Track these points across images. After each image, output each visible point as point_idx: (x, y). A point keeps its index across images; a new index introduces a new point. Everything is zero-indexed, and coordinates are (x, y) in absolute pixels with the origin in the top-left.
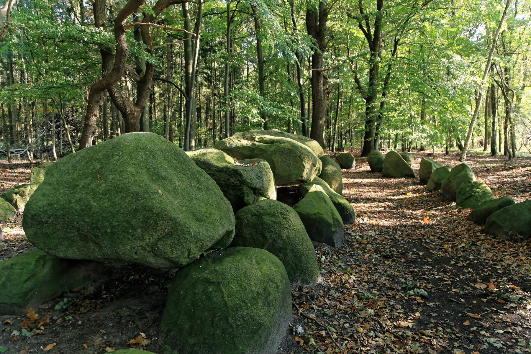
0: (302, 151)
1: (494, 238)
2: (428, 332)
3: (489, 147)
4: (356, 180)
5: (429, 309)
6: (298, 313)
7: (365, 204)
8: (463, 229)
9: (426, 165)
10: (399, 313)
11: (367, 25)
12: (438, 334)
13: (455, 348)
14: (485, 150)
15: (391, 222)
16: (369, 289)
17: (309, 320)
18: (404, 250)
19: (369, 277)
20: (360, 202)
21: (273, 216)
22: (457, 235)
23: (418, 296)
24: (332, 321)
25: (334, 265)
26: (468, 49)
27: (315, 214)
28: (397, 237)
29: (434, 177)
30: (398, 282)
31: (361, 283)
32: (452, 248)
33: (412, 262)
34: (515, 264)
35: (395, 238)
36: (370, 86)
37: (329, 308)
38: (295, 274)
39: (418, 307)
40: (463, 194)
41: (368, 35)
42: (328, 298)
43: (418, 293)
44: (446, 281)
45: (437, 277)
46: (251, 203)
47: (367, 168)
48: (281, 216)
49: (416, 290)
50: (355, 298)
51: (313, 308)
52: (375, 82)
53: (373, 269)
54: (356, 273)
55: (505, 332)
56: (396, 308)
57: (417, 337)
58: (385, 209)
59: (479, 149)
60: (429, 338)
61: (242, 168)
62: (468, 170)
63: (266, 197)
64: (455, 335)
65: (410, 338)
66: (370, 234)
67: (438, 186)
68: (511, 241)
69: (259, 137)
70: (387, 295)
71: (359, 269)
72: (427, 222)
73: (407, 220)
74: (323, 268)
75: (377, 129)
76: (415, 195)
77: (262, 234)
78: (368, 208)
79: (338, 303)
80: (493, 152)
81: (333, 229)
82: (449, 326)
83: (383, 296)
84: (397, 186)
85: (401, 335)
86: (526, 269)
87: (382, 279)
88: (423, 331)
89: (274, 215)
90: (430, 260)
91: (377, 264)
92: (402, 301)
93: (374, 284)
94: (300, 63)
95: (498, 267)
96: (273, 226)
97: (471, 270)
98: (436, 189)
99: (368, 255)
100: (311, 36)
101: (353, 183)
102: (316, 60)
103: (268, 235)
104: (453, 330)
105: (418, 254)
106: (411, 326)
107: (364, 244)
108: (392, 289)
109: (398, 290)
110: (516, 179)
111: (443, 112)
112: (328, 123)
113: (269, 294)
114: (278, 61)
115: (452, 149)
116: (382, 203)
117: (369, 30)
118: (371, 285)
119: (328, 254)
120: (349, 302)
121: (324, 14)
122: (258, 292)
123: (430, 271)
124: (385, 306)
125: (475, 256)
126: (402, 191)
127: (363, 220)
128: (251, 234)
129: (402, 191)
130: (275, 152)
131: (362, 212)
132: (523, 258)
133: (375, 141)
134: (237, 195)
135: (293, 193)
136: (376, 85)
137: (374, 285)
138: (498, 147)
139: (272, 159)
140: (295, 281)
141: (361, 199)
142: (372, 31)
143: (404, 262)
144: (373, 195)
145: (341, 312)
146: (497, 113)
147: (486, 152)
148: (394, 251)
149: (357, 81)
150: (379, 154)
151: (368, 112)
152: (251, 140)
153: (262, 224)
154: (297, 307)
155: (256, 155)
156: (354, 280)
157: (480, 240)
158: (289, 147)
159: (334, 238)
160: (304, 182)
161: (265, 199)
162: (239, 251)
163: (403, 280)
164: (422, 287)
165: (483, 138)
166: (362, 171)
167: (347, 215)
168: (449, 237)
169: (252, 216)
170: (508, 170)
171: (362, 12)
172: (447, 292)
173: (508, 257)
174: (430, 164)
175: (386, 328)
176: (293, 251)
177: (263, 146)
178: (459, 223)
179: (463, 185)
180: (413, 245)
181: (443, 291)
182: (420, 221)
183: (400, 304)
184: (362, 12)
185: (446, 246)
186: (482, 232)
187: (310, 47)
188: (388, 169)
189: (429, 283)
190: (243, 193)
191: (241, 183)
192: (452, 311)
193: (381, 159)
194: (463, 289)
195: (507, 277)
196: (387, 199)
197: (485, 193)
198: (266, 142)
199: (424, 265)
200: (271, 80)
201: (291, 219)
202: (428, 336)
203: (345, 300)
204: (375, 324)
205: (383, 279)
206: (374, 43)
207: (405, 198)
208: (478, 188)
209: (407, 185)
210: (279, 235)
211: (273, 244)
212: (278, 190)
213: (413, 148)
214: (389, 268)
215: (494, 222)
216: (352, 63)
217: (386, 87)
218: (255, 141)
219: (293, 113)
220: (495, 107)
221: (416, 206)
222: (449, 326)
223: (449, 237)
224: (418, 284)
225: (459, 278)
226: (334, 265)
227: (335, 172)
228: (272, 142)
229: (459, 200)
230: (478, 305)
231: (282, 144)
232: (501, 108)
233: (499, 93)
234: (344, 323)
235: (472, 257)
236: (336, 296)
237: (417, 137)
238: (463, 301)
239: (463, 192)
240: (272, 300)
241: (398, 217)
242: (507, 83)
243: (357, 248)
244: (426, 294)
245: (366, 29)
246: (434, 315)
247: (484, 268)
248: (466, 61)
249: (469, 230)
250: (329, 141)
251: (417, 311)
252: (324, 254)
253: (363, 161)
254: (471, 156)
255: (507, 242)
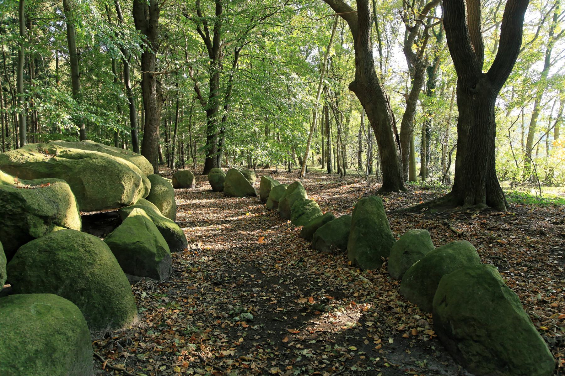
0: (120, 169)
1: (319, 253)
2: (249, 356)
3: (326, 165)
4: (194, 201)
5: (253, 332)
6: (103, 366)
7: (201, 228)
8: (294, 247)
9: (265, 183)
10: (222, 343)
11: (206, 30)
12: (258, 357)
13: (273, 366)
14: (323, 168)
15: (227, 246)
16: (194, 323)
17: (117, 372)
18: (235, 274)
19: (195, 309)
20: (196, 226)
21: (71, 250)
22: (288, 253)
23: (244, 321)
24: (146, 367)
25: (157, 300)
26: (304, 69)
27: (134, 243)
28: (231, 261)
29: (272, 196)
30: (226, 310)
31: (186, 317)
32: (282, 267)
33: (243, 286)
34: (333, 276)
35: (229, 262)
36: (210, 97)
37: (143, 353)
38: (103, 319)
39: (243, 333)
40: (296, 212)
41: (207, 40)
42: (145, 342)
43: (244, 317)
44: (272, 301)
45: (265, 298)
46: (41, 235)
47: (208, 187)
48: (81, 249)
49: (243, 315)
50: (176, 336)
51: (123, 356)
52: (217, 94)
53: (201, 299)
54: (181, 306)
55: (317, 342)
56: (220, 337)
57: (237, 364)
58: (222, 231)
59: (318, 167)
60: (249, 363)
61: (25, 190)
62: (300, 187)
63: (65, 227)
64: (273, 354)
65: (231, 367)
66: (203, 260)
67: (276, 204)
68: (332, 254)
69: (61, 150)
70: (212, 326)
71: (185, 300)
72: (262, 242)
73: (243, 241)
74: (143, 306)
75: (220, 144)
76: (254, 215)
77: (55, 275)
78: (204, 232)
79: (155, 344)
80: (329, 170)
81: (157, 259)
82: (270, 346)
83: (208, 327)
84: (238, 206)
85: (222, 366)
86: (341, 280)
87: (209, 309)
88: (244, 357)
89: (72, 249)
90: (260, 282)
91: (205, 294)
92: (228, 329)
93: (200, 315)
94: (129, 61)
95: (319, 280)
96: (70, 263)
97: (296, 287)
98: (274, 207)
99: (197, 284)
100: (139, 31)
101: (190, 205)
102: (146, 61)
103: (63, 275)
104: (272, 349)
105: (250, 276)
106: (233, 354)
107: (194, 272)
108: (218, 318)
109: (225, 318)
110: (343, 195)
111: (284, 130)
112: (166, 135)
113: (54, 350)
114: (99, 58)
115: (294, 167)
116: (220, 226)
117: (207, 34)
118: (197, 317)
119: (150, 289)
120: (169, 341)
121: (155, 11)
122: (37, 351)
123: (259, 293)
124: (209, 338)
125: (301, 272)
126: (242, 210)
127: (197, 245)
128: (38, 276)
129: (242, 210)
130: (84, 170)
131: (196, 236)
132: (339, 270)
133: (218, 157)
134: (19, 227)
135: (104, 219)
136: (217, 97)
137: (200, 317)
138: (333, 165)
139: (80, 178)
140: (103, 327)
141: (198, 222)
142: (212, 38)
143: (235, 287)
144: (211, 216)
145: (158, 354)
146: (330, 134)
147: (323, 170)
148: (225, 277)
149: (197, 90)
150: (221, 172)
151: (210, 125)
152: (50, 154)
153: (55, 261)
154: (102, 358)
155: (57, 172)
156: (178, 315)
157: (307, 256)
158: (103, 163)
159: (158, 269)
160: (124, 205)
161: (63, 228)
162: (12, 302)
163: (231, 307)
164: (249, 311)
165: (320, 156)
166: (203, 191)
167: (175, 241)
168: (281, 256)
169: (40, 252)
170: (337, 187)
171: (199, 14)
172: (272, 312)
173: (329, 269)
174: (270, 182)
175: (207, 362)
176: (99, 291)
177: (66, 161)
178: (292, 241)
179: (296, 203)
180: (247, 267)
181: (268, 312)
182: (256, 242)
183: (225, 333)
184: (199, 14)
185: (277, 266)
186: (310, 247)
187: (139, 44)
188: (227, 187)
189: (256, 306)
190: (27, 223)
191: (23, 210)
192: (274, 331)
193: (223, 177)
194: (287, 306)
195: (325, 289)
196: (226, 221)
197: (315, 210)
198: (71, 157)
199: (254, 287)
200: (90, 79)
201: (97, 252)
202: (249, 361)
203: (164, 339)
204: (195, 359)
205: (211, 308)
206: (213, 50)
207: (245, 219)
208: (309, 206)
209: (247, 204)
210: (79, 274)
211: (71, 285)
212: (83, 218)
213: (259, 165)
214: (219, 295)
215: (319, 238)
216: (191, 70)
217: (227, 99)
218: (55, 155)
219: (116, 122)
220: (329, 127)
221: (254, 227)
222: (270, 346)
223: (281, 256)
224: (246, 309)
225: (285, 295)
226: (157, 300)
227: (166, 192)
228: (80, 157)
229: (293, 218)
230: (297, 320)
231: (94, 160)
232: (334, 129)
233: (331, 114)
234: (160, 366)
235: (298, 274)
236: (154, 336)
237: (261, 155)
238: (285, 318)
239: (296, 210)
240: (58, 356)
241: (235, 240)
242: (337, 105)
243: (186, 278)
244: (252, 317)
245: (204, 33)
246: (257, 337)
247: (308, 283)
248: (302, 80)
249: (299, 247)
250: (168, 156)
251: (241, 336)
252: (145, 290)
253: (205, 180)
254: (311, 174)
255: (329, 256)
